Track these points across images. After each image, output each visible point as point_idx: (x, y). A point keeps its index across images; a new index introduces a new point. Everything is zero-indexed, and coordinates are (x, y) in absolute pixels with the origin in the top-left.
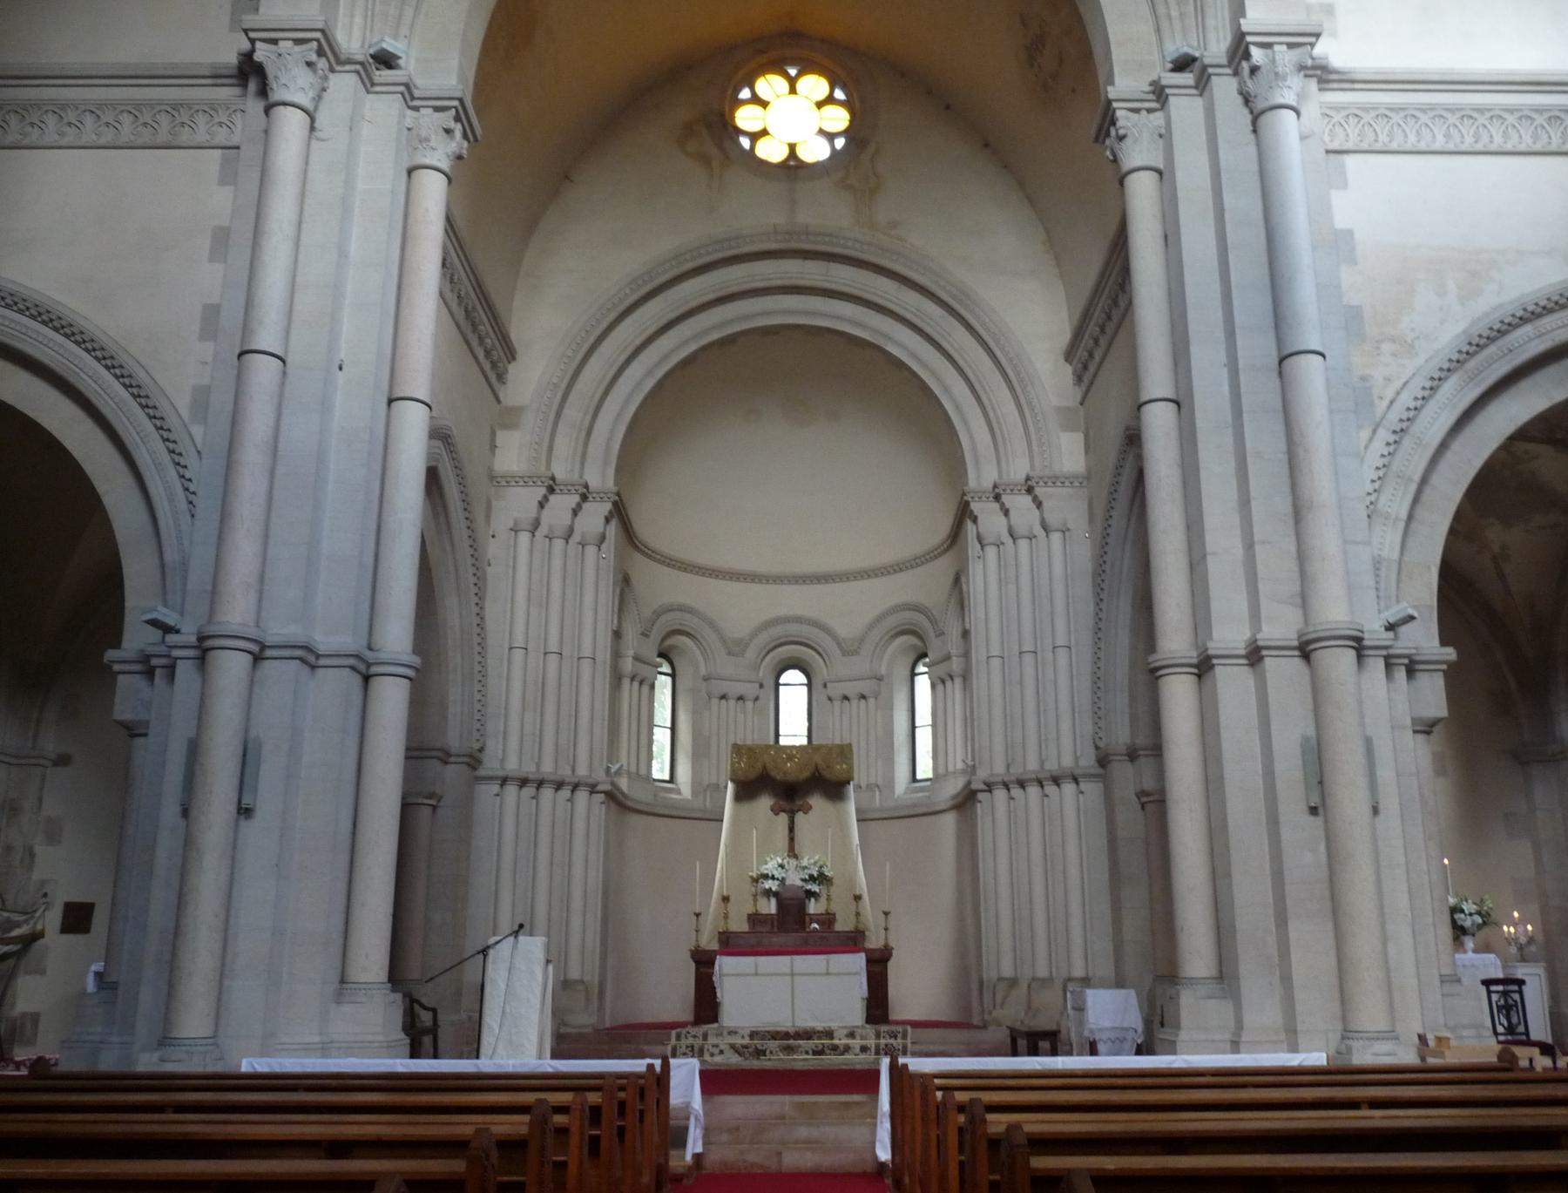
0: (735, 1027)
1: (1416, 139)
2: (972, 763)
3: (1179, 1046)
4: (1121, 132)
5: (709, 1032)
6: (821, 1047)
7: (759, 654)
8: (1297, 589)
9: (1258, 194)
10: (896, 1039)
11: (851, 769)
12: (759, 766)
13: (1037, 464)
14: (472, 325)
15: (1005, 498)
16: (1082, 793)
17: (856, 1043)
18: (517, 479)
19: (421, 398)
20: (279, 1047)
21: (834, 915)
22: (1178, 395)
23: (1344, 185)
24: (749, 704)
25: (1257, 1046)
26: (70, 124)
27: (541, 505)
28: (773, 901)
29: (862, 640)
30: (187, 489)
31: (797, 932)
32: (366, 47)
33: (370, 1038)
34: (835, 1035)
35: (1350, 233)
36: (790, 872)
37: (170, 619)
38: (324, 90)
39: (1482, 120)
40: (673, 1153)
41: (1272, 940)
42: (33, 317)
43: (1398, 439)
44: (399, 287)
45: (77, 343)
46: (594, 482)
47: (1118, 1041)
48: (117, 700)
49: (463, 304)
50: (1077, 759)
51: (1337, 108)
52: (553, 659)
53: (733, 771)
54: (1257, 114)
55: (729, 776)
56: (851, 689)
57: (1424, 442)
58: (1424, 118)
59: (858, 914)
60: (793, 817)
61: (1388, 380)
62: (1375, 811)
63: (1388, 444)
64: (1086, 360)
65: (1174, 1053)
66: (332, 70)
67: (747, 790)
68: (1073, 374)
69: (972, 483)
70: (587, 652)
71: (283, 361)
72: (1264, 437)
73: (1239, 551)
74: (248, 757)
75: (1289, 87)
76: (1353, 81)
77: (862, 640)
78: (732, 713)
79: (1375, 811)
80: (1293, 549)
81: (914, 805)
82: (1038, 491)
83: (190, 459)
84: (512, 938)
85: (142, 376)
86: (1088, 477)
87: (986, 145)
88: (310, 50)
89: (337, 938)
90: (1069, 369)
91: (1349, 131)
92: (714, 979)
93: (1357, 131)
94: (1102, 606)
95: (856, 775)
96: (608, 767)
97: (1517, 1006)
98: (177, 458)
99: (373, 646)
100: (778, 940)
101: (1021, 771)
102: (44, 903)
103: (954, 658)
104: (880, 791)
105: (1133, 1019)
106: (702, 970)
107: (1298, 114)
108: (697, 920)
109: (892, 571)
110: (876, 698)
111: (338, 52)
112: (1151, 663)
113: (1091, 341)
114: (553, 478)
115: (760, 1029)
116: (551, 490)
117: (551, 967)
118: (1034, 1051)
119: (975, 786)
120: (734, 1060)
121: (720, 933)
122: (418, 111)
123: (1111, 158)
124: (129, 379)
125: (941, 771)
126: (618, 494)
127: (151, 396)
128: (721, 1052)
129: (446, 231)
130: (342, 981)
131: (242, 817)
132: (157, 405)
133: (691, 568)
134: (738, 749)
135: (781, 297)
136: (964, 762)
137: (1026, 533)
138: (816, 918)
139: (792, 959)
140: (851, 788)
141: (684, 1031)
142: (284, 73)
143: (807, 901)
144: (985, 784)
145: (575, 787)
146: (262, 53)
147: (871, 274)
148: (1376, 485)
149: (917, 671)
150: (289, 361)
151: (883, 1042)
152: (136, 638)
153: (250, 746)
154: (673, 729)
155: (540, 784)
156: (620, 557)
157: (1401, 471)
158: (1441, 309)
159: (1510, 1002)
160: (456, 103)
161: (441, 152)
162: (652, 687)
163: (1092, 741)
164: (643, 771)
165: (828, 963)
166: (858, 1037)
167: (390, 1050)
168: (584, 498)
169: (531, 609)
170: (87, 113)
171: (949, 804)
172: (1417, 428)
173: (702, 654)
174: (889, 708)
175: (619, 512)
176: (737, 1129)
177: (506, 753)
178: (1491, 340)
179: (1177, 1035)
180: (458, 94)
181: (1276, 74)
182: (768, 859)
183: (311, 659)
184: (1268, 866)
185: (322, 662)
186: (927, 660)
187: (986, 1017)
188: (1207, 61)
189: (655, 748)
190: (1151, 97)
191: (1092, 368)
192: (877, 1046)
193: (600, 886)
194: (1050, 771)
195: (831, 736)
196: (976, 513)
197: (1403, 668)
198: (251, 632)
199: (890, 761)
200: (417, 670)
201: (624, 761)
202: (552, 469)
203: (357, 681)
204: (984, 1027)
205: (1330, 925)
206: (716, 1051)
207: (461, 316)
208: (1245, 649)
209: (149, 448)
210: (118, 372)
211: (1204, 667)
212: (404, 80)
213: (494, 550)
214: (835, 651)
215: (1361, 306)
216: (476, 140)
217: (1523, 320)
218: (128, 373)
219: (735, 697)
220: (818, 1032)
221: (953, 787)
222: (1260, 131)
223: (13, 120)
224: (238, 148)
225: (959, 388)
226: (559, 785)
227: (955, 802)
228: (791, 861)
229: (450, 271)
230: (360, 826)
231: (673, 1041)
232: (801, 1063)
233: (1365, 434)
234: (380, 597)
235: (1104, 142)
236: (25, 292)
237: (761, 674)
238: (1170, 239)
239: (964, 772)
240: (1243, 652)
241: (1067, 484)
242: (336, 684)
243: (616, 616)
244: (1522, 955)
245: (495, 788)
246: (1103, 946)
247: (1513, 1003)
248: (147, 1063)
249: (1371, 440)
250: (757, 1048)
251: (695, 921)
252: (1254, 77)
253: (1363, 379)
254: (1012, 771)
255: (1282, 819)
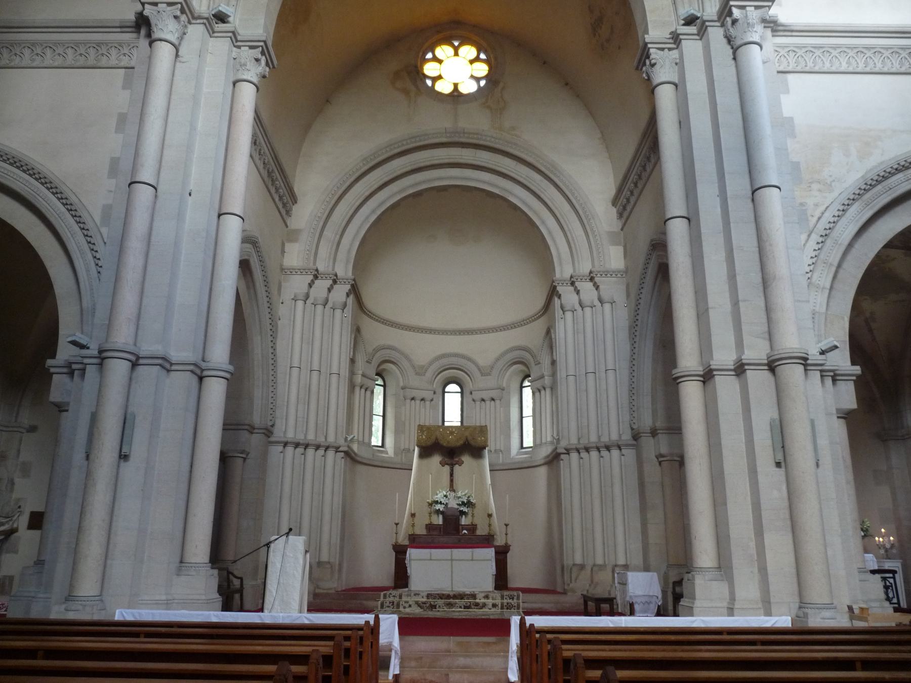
0: (419, 591)
1: (830, 65)
2: (558, 437)
3: (696, 611)
4: (653, 61)
5: (403, 594)
6: (469, 604)
7: (434, 375)
8: (766, 329)
9: (737, 95)
10: (513, 600)
11: (486, 441)
12: (433, 438)
13: (596, 263)
14: (272, 180)
15: (577, 284)
16: (623, 455)
17: (490, 602)
18: (297, 271)
19: (238, 213)
20: (141, 602)
21: (476, 525)
22: (688, 213)
23: (787, 91)
24: (428, 403)
25: (745, 611)
26: (37, 54)
27: (310, 286)
28: (441, 517)
29: (492, 368)
30: (97, 265)
31: (454, 535)
32: (211, 9)
33: (198, 597)
34: (477, 596)
35: (791, 119)
36: (450, 500)
37: (83, 340)
38: (185, 34)
39: (869, 54)
40: (381, 673)
41: (752, 544)
42: (11, 164)
43: (823, 240)
44: (227, 150)
45: (36, 179)
46: (341, 273)
47: (646, 603)
48: (52, 389)
49: (267, 169)
50: (620, 435)
51: (783, 47)
52: (315, 374)
53: (418, 440)
54: (735, 47)
55: (416, 444)
56: (486, 395)
57: (839, 242)
58: (834, 53)
59: (490, 525)
60: (453, 468)
61: (816, 205)
62: (818, 465)
63: (818, 243)
64: (626, 204)
65: (692, 615)
66: (190, 23)
67: (426, 452)
68: (617, 213)
69: (558, 275)
70: (335, 370)
71: (156, 189)
72: (744, 239)
73: (728, 307)
74: (126, 423)
75: (755, 31)
76: (792, 31)
77: (492, 368)
78: (417, 408)
79: (818, 465)
80: (762, 304)
81: (522, 462)
82: (597, 279)
83: (100, 247)
84: (284, 537)
85: (73, 199)
86: (626, 271)
87: (567, 84)
88: (177, 9)
89: (179, 534)
90: (614, 210)
91: (790, 60)
92: (406, 562)
93: (794, 61)
94: (636, 345)
95: (489, 443)
96: (346, 437)
97: (892, 586)
98: (92, 246)
99: (205, 360)
100: (443, 539)
101: (586, 442)
102: (18, 512)
103: (546, 377)
104: (502, 454)
105: (656, 590)
106: (399, 556)
107: (761, 48)
108: (507, 528)
109: (510, 328)
110: (500, 400)
111: (193, 11)
112: (673, 375)
113: (629, 193)
114: (317, 270)
115: (433, 592)
116: (316, 277)
117: (308, 555)
118: (599, 613)
119: (559, 451)
120: (416, 611)
121: (409, 535)
122: (240, 49)
123: (646, 78)
124: (66, 200)
125: (538, 442)
126: (354, 280)
127: (78, 210)
128: (410, 606)
129: (254, 118)
130: (181, 562)
131: (122, 460)
132: (82, 215)
133: (395, 325)
134: (421, 428)
135: (448, 170)
136: (552, 436)
137: (589, 304)
138: (464, 528)
139: (452, 551)
140: (486, 451)
141: (388, 593)
142: (161, 22)
143: (460, 517)
144: (566, 449)
145: (327, 448)
146: (148, 11)
147: (500, 156)
148: (811, 267)
149: (524, 385)
150: (159, 190)
151: (505, 601)
152: (65, 352)
153: (128, 416)
154: (384, 416)
155: (306, 446)
156: (355, 318)
157: (826, 260)
158: (847, 164)
159: (888, 584)
160: (262, 44)
161: (253, 72)
162: (372, 392)
163: (629, 426)
164: (366, 441)
165: (472, 554)
166: (491, 599)
167: (207, 605)
168: (335, 282)
169: (303, 345)
170: (48, 48)
171: (542, 462)
172: (835, 234)
173: (401, 373)
174: (508, 406)
175: (355, 290)
176: (421, 658)
177: (287, 429)
178: (879, 182)
179: (693, 603)
180: (264, 38)
181: (748, 24)
182: (438, 492)
183: (167, 366)
184: (749, 498)
185: (174, 367)
186: (530, 378)
187: (566, 587)
188: (705, 18)
189: (373, 429)
190: (671, 41)
191: (629, 208)
192: (502, 604)
193: (340, 507)
194: (603, 442)
195: (476, 420)
196: (560, 293)
197: (830, 378)
198: (131, 348)
199: (508, 437)
200: (232, 374)
201: (355, 434)
202: (317, 265)
203: (195, 380)
204: (565, 593)
205: (790, 535)
206: (407, 605)
207: (265, 174)
208: (734, 365)
209: (77, 241)
210: (59, 196)
211: (707, 376)
212: (232, 29)
213: (283, 311)
214: (477, 373)
215: (799, 162)
216: (274, 67)
217: (898, 171)
218: (75, 209)
219: (420, 399)
220: (467, 595)
221: (546, 451)
222: (738, 58)
223: (5, 51)
224: (133, 68)
225: (551, 222)
226: (317, 447)
227: (547, 459)
228: (451, 494)
229: (259, 148)
230: (195, 467)
231: (382, 599)
232: (457, 614)
233: (804, 237)
234: (210, 330)
235: (641, 69)
236: (6, 149)
237: (434, 386)
238: (684, 123)
239: (552, 443)
240: (732, 367)
241: (614, 275)
242: (182, 380)
243: (352, 350)
244: (887, 555)
245: (280, 448)
246: (636, 546)
247: (889, 585)
248: (57, 613)
249: (807, 241)
250: (431, 604)
251: (395, 528)
252: (734, 26)
253: (802, 204)
254: (581, 442)
255: (759, 469)
